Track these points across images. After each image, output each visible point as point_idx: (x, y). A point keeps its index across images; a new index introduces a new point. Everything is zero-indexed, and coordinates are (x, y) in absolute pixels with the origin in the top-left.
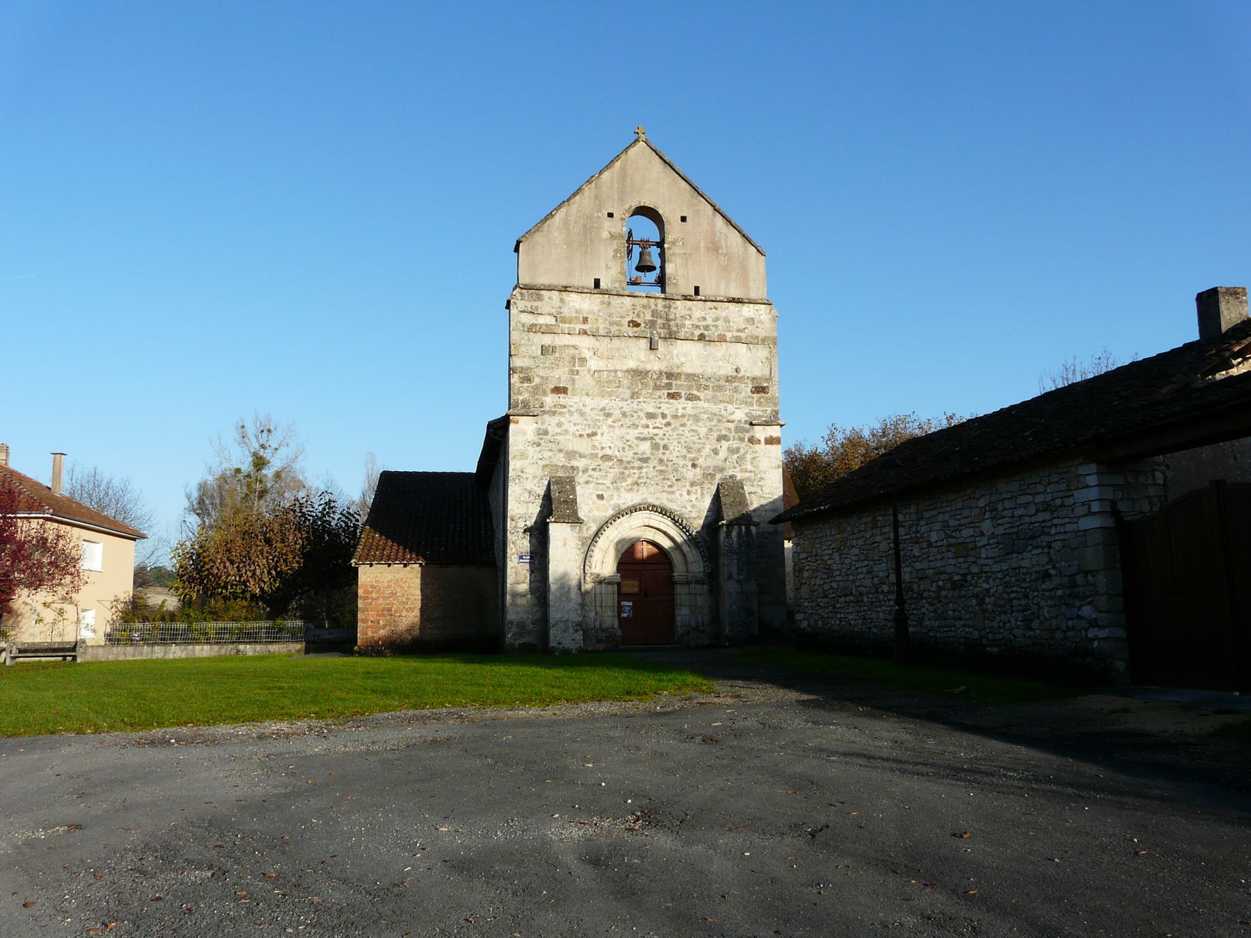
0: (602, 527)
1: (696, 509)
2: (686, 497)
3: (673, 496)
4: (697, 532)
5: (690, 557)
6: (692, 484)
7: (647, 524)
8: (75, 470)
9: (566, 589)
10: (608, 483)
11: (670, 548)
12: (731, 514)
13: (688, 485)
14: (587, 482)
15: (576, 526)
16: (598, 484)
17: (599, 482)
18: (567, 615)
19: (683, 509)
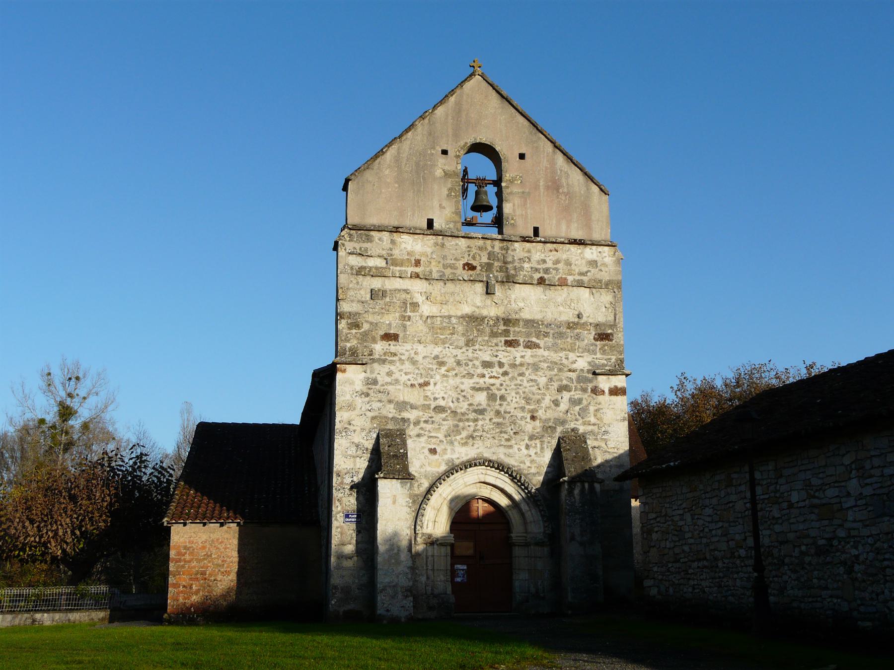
0: (434, 484)
1: (535, 465)
2: (524, 451)
3: (511, 451)
4: (536, 489)
5: (528, 515)
6: (531, 438)
9: (396, 551)
10: (441, 436)
11: (508, 506)
12: (573, 470)
13: (527, 438)
15: (407, 483)
16: (431, 437)
19: (521, 465)
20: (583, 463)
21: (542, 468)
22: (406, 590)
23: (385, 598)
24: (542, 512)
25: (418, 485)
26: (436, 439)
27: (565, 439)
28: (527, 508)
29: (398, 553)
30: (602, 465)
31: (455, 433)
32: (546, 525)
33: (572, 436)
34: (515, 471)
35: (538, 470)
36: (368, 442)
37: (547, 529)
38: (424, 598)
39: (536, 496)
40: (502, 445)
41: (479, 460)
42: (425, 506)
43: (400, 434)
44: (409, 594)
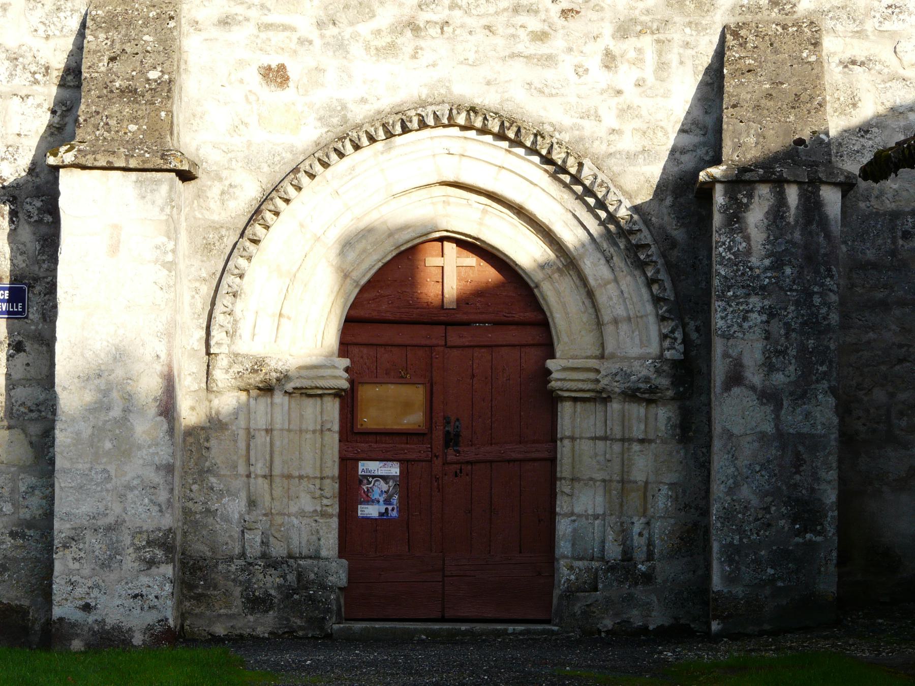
0: (275, 189)
1: (637, 124)
2: (599, 76)
3: (549, 74)
4: (636, 209)
5: (608, 297)
6: (623, 30)
7: (451, 178)
8: (462, 153)
9: (116, 413)
10: (306, 28)
11: (542, 267)
12: (752, 140)
13: (608, 29)
14: (225, 22)
15: (158, 182)
16: (268, 27)
17: (269, 19)
18: (117, 509)
19: (585, 123)
20: (792, 118)
21: (660, 134)
22: (149, 543)
23: (77, 565)
24: (655, 288)
25: (223, 193)
26: (287, 34)
27: (743, 33)
28: (604, 271)
29: (125, 419)
30: (877, 126)
31: (352, 13)
32: (665, 331)
33: (768, 23)
34: (559, 143)
35: (646, 143)
36: (52, 42)
37: (667, 343)
38: (233, 568)
39: (631, 232)
40: (519, 55)
41: (434, 108)
42: (242, 262)
43: (158, 17)
44: (159, 554)
